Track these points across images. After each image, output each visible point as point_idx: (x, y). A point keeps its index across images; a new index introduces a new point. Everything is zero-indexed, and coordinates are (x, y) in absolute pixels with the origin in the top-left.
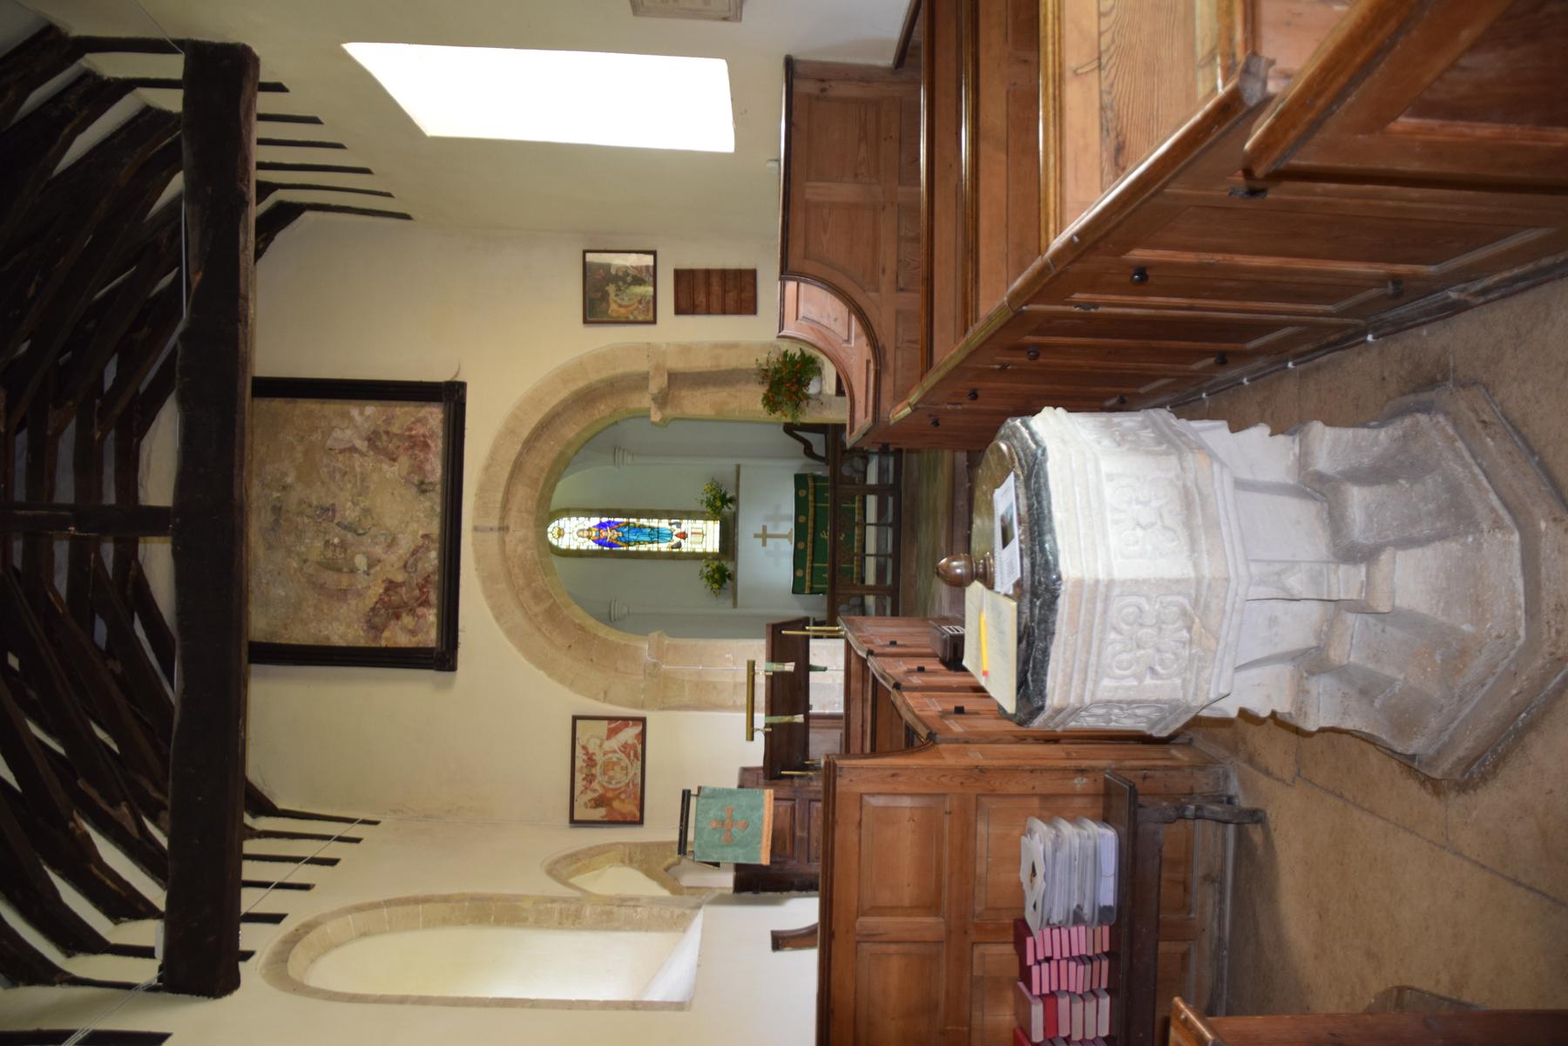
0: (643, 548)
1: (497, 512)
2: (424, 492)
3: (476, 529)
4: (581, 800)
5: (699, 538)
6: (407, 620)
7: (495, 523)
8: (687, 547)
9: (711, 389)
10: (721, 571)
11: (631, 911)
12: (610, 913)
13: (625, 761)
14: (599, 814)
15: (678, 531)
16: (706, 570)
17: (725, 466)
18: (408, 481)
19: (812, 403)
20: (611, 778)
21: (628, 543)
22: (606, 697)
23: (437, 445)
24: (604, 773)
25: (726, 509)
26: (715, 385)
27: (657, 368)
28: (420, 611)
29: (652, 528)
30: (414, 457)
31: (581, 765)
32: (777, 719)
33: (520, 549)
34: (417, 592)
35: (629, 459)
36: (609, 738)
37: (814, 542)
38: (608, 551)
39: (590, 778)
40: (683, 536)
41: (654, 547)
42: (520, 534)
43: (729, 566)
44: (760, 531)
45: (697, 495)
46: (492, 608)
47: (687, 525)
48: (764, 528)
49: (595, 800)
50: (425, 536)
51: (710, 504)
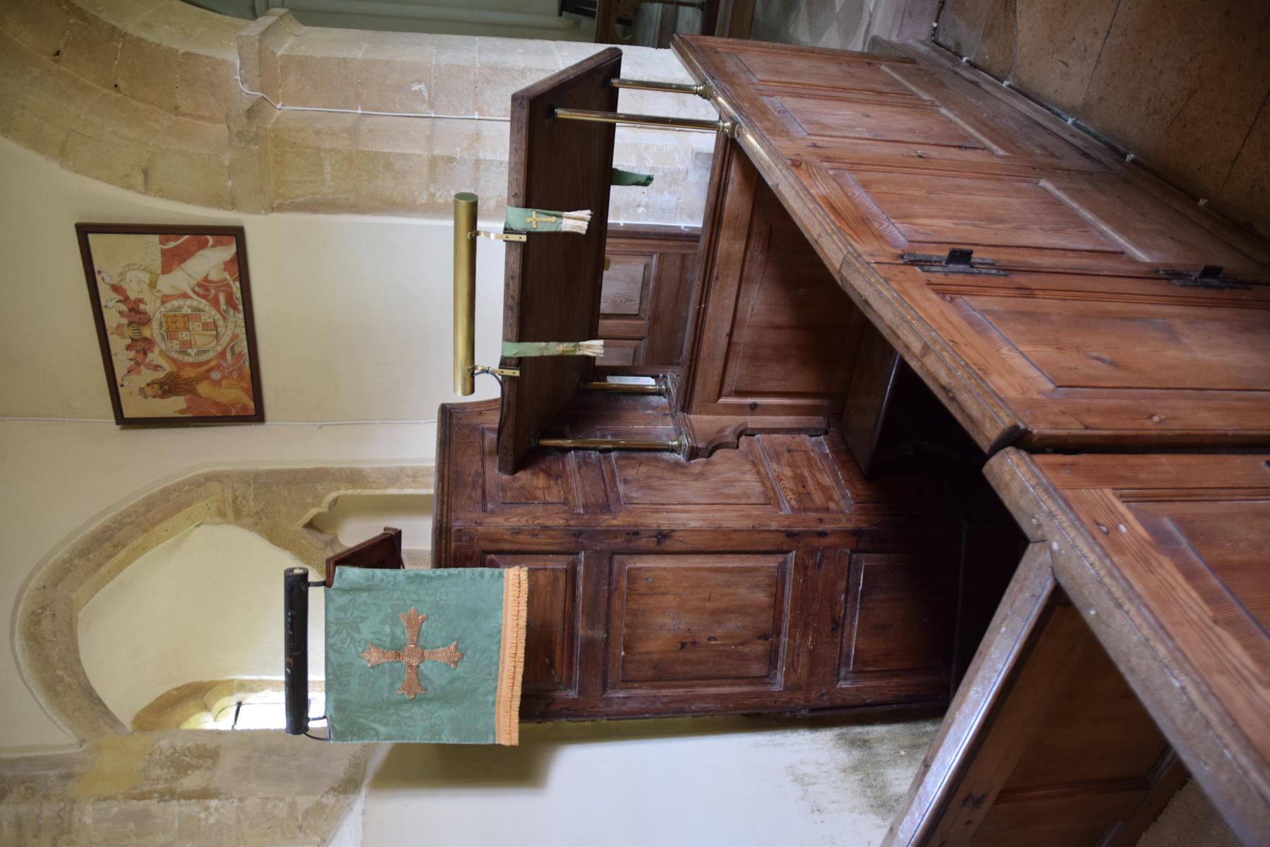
4: (130, 388)
11: (193, 807)
12: (143, 817)
13: (210, 314)
14: (174, 405)
20: (185, 346)
22: (148, 182)
24: (170, 335)
31: (117, 327)
32: (532, 349)
36: (166, 269)
39: (142, 346)
49: (161, 383)
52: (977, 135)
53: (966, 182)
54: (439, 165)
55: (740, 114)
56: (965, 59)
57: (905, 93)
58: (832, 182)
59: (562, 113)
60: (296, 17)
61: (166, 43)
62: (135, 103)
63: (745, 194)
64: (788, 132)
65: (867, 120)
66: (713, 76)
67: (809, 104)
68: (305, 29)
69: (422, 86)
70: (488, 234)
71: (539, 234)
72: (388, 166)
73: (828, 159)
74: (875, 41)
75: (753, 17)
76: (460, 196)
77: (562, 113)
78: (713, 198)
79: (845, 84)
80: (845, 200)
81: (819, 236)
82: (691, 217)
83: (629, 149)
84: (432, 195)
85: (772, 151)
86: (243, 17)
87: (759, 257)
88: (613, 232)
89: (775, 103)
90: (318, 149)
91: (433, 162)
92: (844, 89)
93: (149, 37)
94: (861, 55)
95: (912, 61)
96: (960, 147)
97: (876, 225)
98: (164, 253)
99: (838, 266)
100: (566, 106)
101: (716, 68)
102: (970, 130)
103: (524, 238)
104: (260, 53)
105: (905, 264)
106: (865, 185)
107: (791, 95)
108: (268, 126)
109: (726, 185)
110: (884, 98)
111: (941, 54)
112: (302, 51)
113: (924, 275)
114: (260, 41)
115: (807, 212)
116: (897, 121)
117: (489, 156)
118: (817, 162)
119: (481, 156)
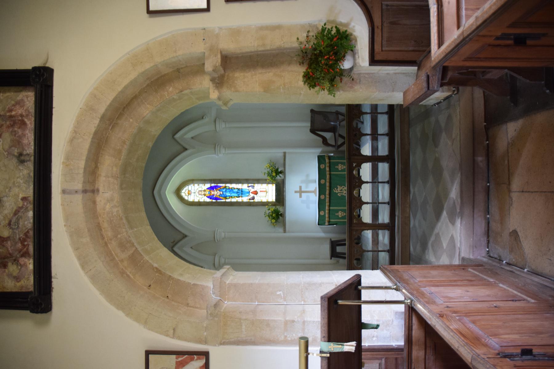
0: (234, 200)
1: (80, 178)
2: (22, 162)
3: (64, 192)
5: (264, 194)
6: (12, 268)
7: (79, 186)
8: (257, 199)
9: (260, 70)
10: (277, 212)
15: (252, 190)
16: (268, 212)
17: (277, 153)
18: (10, 154)
19: (345, 79)
21: (226, 197)
22: (175, 334)
23: (30, 123)
25: (278, 178)
26: (263, 66)
27: (212, 49)
28: (22, 260)
29: (239, 189)
30: (14, 133)
33: (108, 207)
34: (19, 245)
35: (223, 151)
37: (330, 194)
38: (216, 202)
40: (256, 193)
41: (240, 200)
42: (108, 195)
43: (280, 209)
44: (298, 189)
45: (262, 170)
46: (79, 258)
47: (258, 187)
48: (300, 187)
50: (24, 199)
51: (269, 174)
52: (519, 294)
53: (520, 316)
54: (289, 324)
55: (413, 296)
56: (504, 262)
57: (482, 279)
58: (459, 322)
59: (340, 302)
60: (233, 268)
61: (188, 281)
62: (173, 303)
63: (422, 333)
64: (435, 302)
65: (468, 293)
66: (399, 282)
67: (441, 289)
68: (236, 273)
69: (281, 292)
70: (313, 354)
71: (334, 353)
72: (268, 325)
73: (455, 312)
74: (463, 259)
75: (410, 253)
76: (301, 338)
77: (340, 302)
78: (407, 333)
79: (455, 279)
80: (467, 330)
81: (458, 347)
82: (397, 340)
83: (368, 314)
84: (286, 337)
85: (430, 311)
86: (210, 269)
87: (432, 358)
88: (364, 349)
89: (427, 290)
90: (240, 319)
91: (286, 323)
92: (455, 281)
93: (181, 279)
94: (459, 266)
95: (482, 265)
96: (513, 300)
97: (483, 340)
98: (177, 362)
99: (470, 361)
100: (342, 299)
101: (400, 278)
102: (515, 292)
103: (328, 355)
104: (220, 283)
105: (501, 357)
106: (474, 322)
107: (434, 286)
108: (222, 311)
109: (412, 326)
110: (472, 283)
111: (494, 261)
112: (235, 281)
113: (512, 362)
114: (221, 278)
115: (450, 337)
116: (482, 292)
117: (309, 319)
118: (450, 314)
119: (306, 319)
